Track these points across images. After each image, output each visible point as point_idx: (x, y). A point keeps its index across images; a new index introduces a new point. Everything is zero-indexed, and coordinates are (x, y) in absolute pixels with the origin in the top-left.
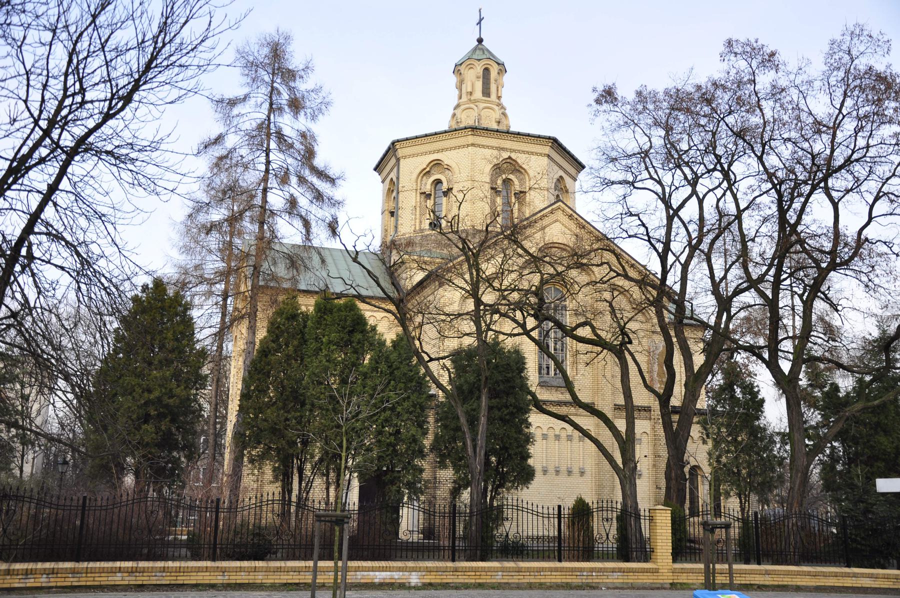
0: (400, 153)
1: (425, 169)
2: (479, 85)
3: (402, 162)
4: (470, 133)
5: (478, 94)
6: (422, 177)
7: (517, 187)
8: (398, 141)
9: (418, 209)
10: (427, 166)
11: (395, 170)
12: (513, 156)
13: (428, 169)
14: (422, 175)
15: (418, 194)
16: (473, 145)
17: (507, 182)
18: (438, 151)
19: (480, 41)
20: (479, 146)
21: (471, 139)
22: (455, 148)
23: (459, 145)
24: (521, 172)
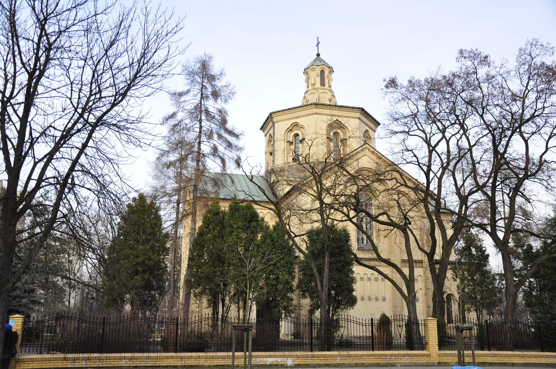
0: (275, 119)
1: (289, 128)
2: (318, 80)
3: (276, 124)
4: (314, 107)
5: (318, 85)
6: (288, 133)
7: (342, 136)
8: (273, 113)
9: (286, 151)
10: (290, 126)
11: (272, 129)
12: (339, 119)
13: (291, 128)
14: (287, 131)
15: (286, 142)
16: (316, 113)
17: (336, 134)
18: (296, 118)
19: (318, 55)
20: (319, 114)
21: (315, 110)
22: (306, 116)
23: (308, 114)
24: (344, 128)
